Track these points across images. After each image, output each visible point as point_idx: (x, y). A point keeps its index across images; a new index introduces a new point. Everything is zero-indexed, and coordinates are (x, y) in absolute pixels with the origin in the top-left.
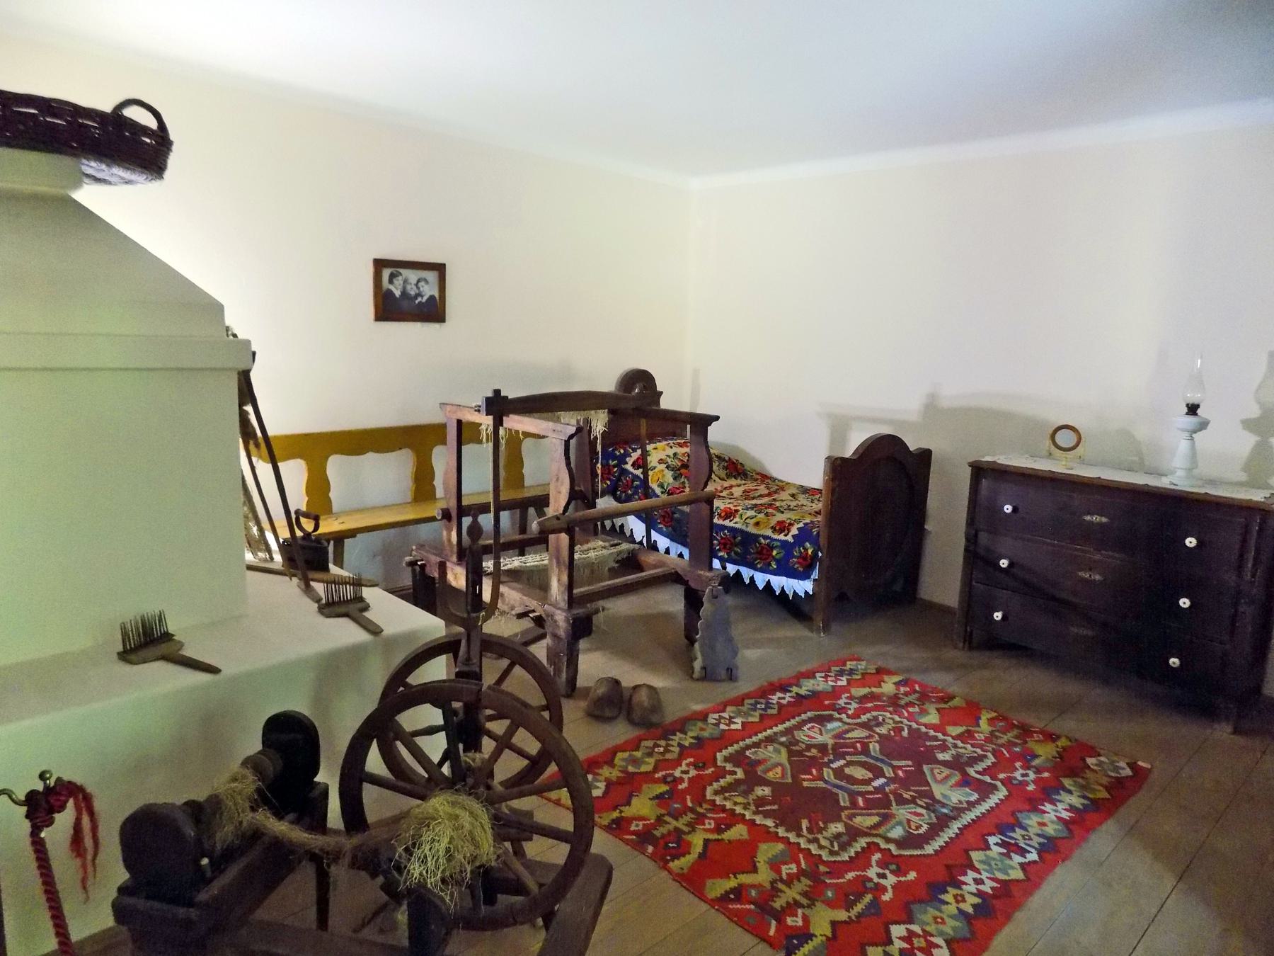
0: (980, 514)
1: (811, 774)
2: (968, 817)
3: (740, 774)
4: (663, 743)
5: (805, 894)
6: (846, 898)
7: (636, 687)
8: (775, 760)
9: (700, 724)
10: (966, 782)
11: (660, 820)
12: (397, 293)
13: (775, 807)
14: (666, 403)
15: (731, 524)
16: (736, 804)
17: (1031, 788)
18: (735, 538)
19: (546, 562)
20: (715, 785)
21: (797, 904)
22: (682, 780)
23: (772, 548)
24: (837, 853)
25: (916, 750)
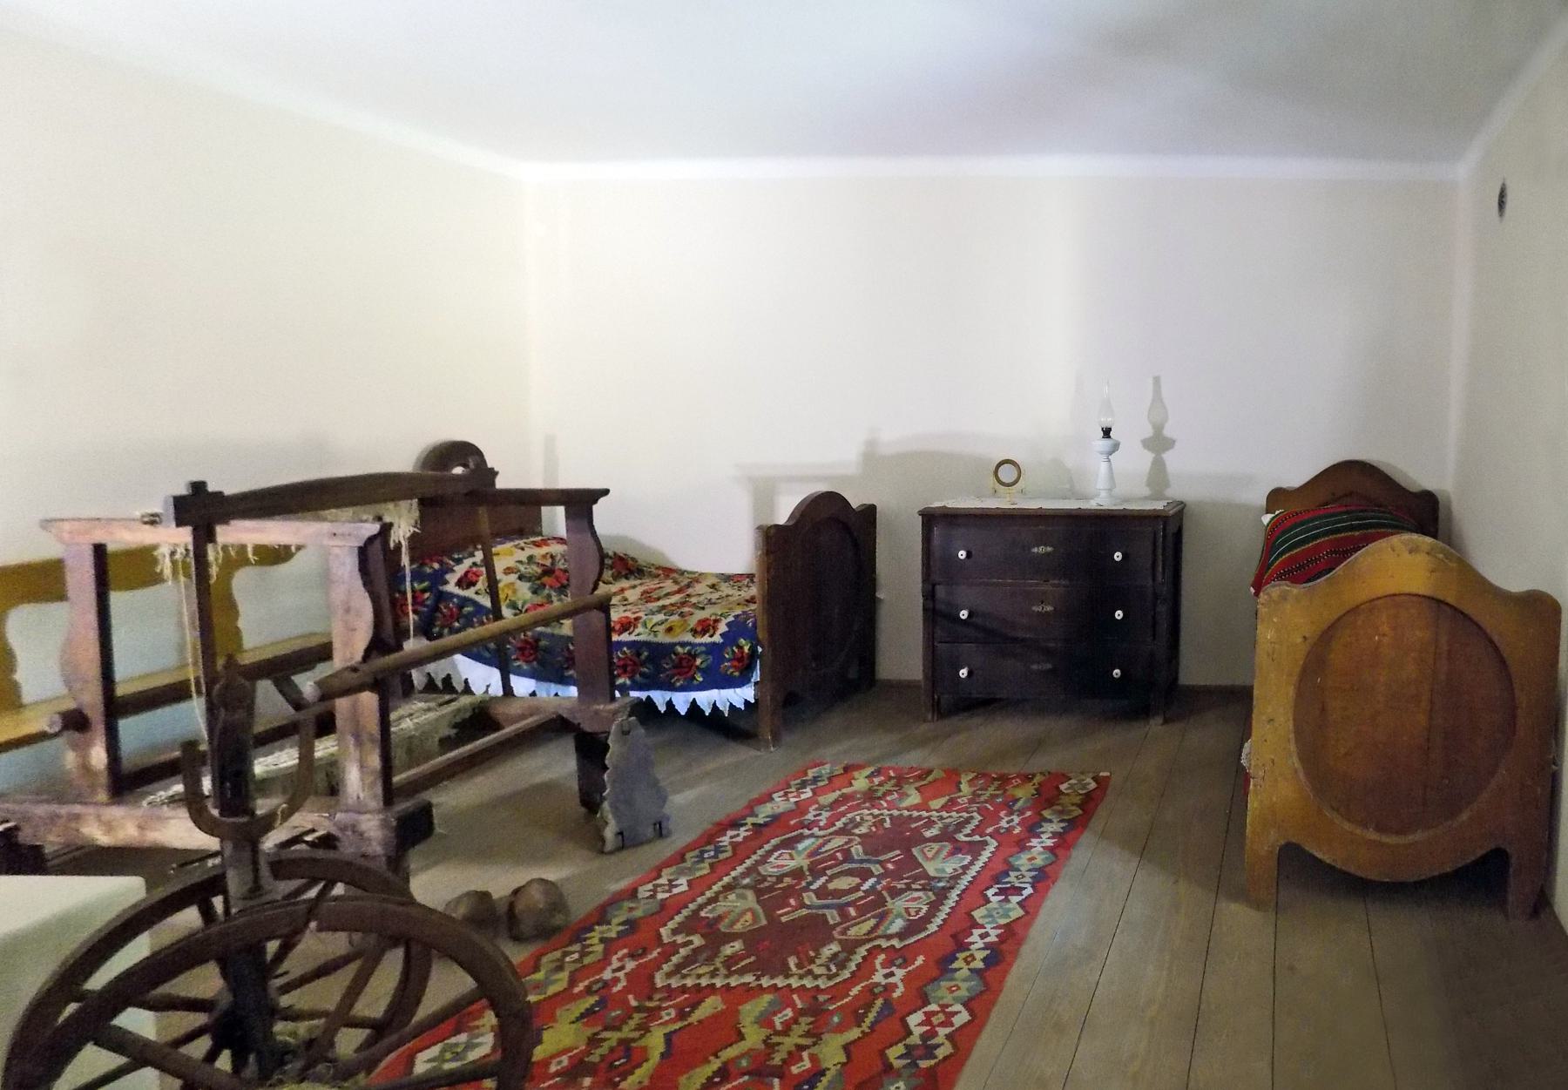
0: (936, 569)
1: (789, 905)
2: (964, 882)
3: (697, 941)
4: (577, 947)
5: (808, 1034)
6: (854, 1016)
7: (516, 892)
8: (741, 909)
9: (627, 904)
10: (958, 848)
11: (594, 1041)
13: (752, 959)
14: (501, 483)
15: (633, 638)
16: (699, 976)
17: (1017, 831)
18: (639, 655)
19: (334, 750)
20: (666, 968)
21: (801, 1048)
22: (616, 980)
23: (695, 657)
24: (837, 975)
25: (903, 837)
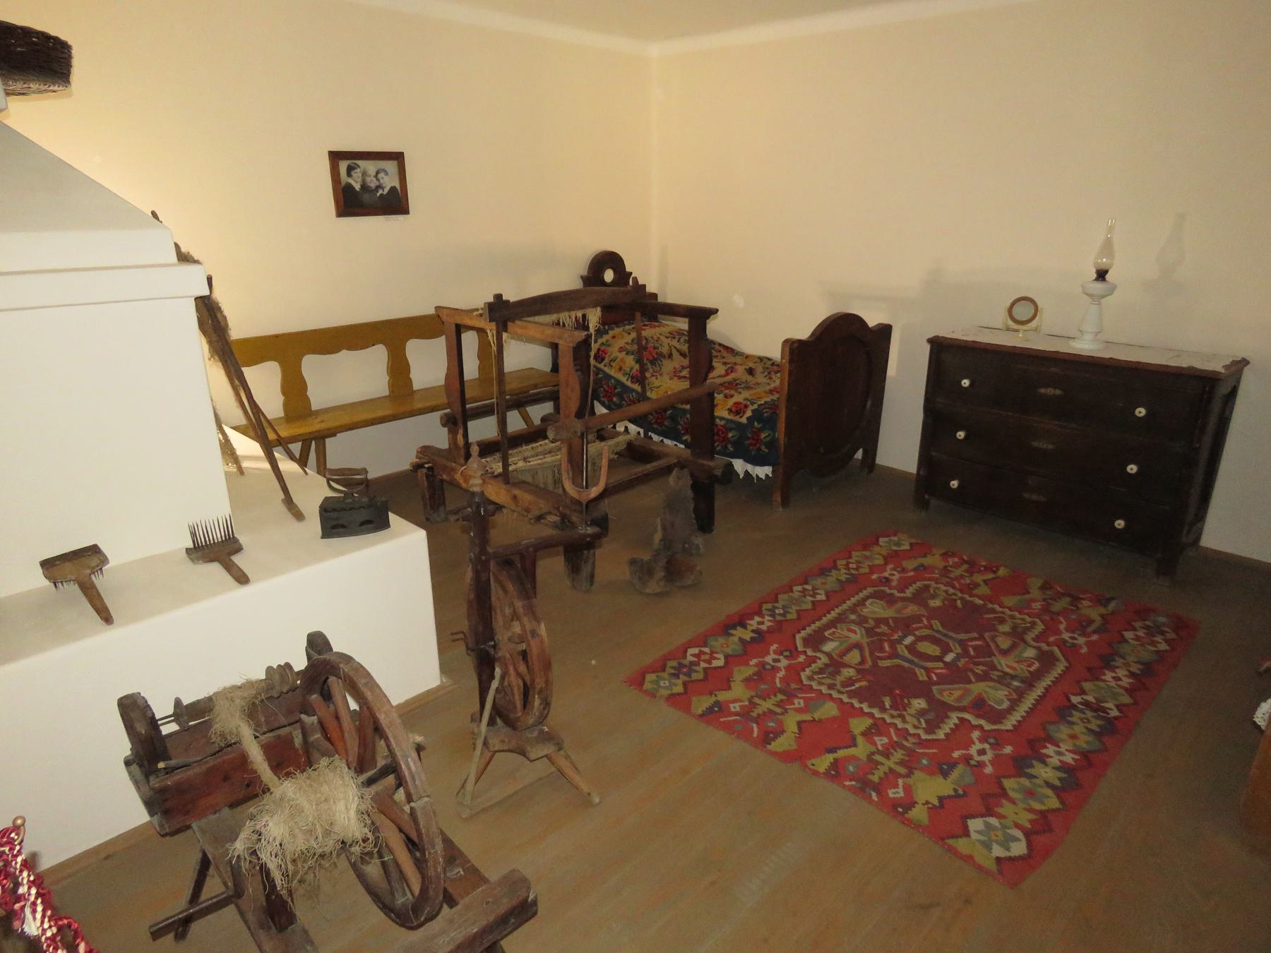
12: (357, 187)
